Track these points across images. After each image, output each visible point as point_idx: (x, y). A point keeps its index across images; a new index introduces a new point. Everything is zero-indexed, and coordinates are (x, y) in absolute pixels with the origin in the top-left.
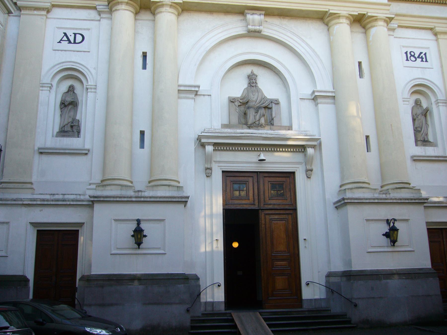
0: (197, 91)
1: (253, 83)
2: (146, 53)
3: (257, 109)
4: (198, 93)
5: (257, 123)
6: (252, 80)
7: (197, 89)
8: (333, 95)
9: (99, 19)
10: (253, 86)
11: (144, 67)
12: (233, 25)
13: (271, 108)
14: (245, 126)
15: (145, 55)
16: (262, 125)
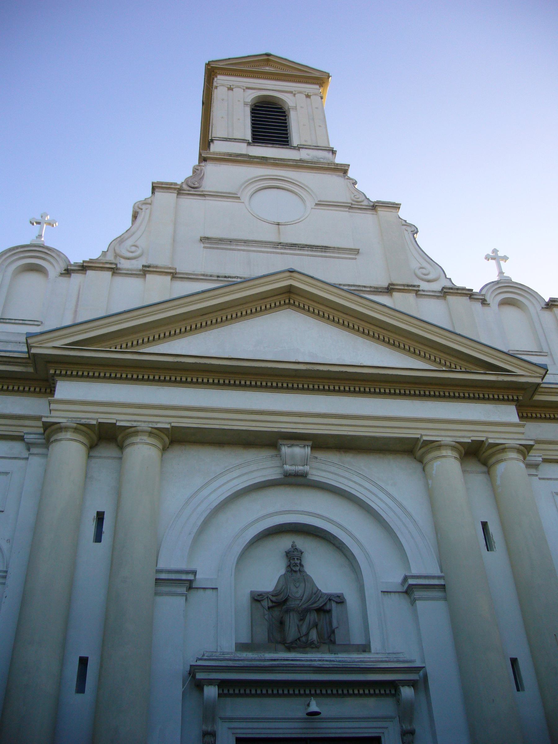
0: (191, 581)
1: (296, 565)
2: (103, 513)
3: (303, 614)
4: (194, 585)
5: (303, 639)
6: (294, 562)
7: (191, 577)
8: (442, 582)
9: (27, 456)
10: (295, 572)
11: (98, 538)
12: (259, 466)
13: (329, 611)
14: (281, 647)
15: (100, 517)
16: (312, 643)
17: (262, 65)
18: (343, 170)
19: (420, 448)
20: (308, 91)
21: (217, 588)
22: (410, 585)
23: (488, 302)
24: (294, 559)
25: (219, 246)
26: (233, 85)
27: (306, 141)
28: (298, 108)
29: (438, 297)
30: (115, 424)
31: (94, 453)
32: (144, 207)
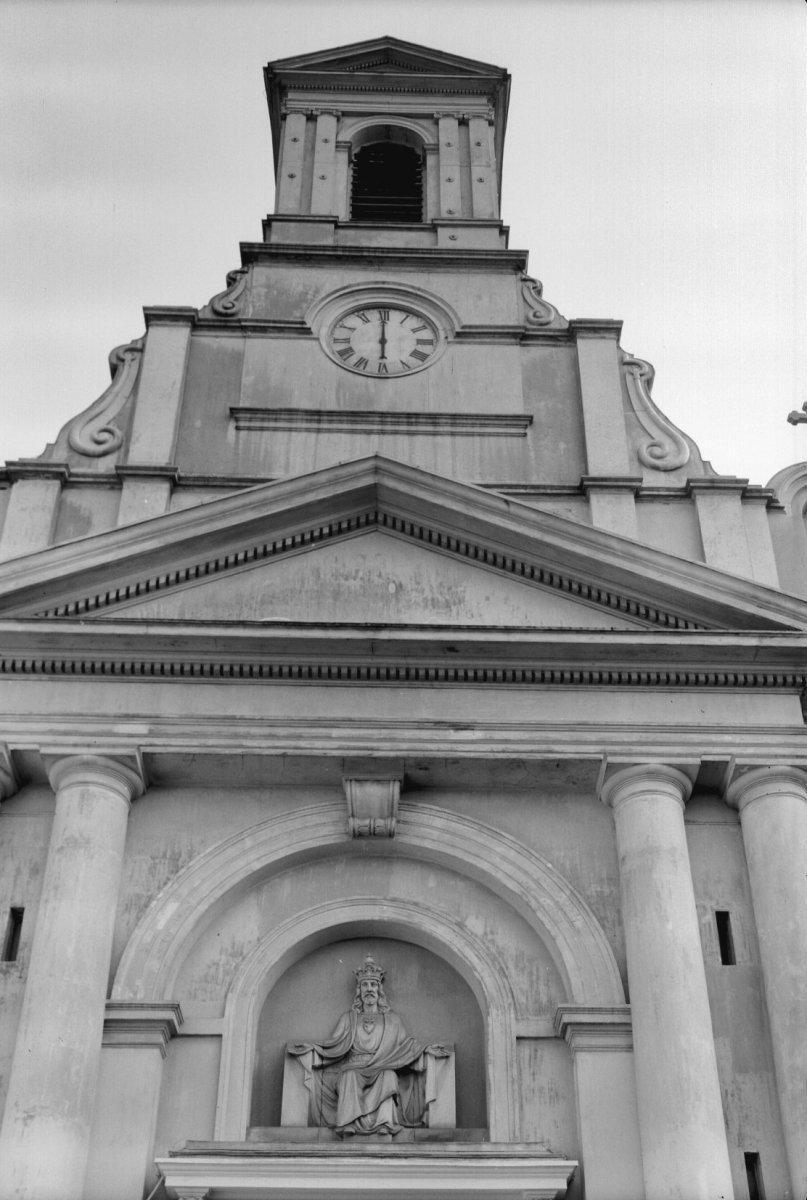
7: (170, 1015)
12: (312, 825)
17: (388, 62)
18: (517, 262)
19: (605, 781)
20: (313, 106)
21: (220, 1036)
22: (566, 1025)
23: (781, 504)
24: (366, 984)
25: (359, 427)
26: (317, 109)
27: (450, 212)
28: (443, 149)
29: (681, 497)
30: (38, 751)
31: (144, 804)
32: (128, 356)
